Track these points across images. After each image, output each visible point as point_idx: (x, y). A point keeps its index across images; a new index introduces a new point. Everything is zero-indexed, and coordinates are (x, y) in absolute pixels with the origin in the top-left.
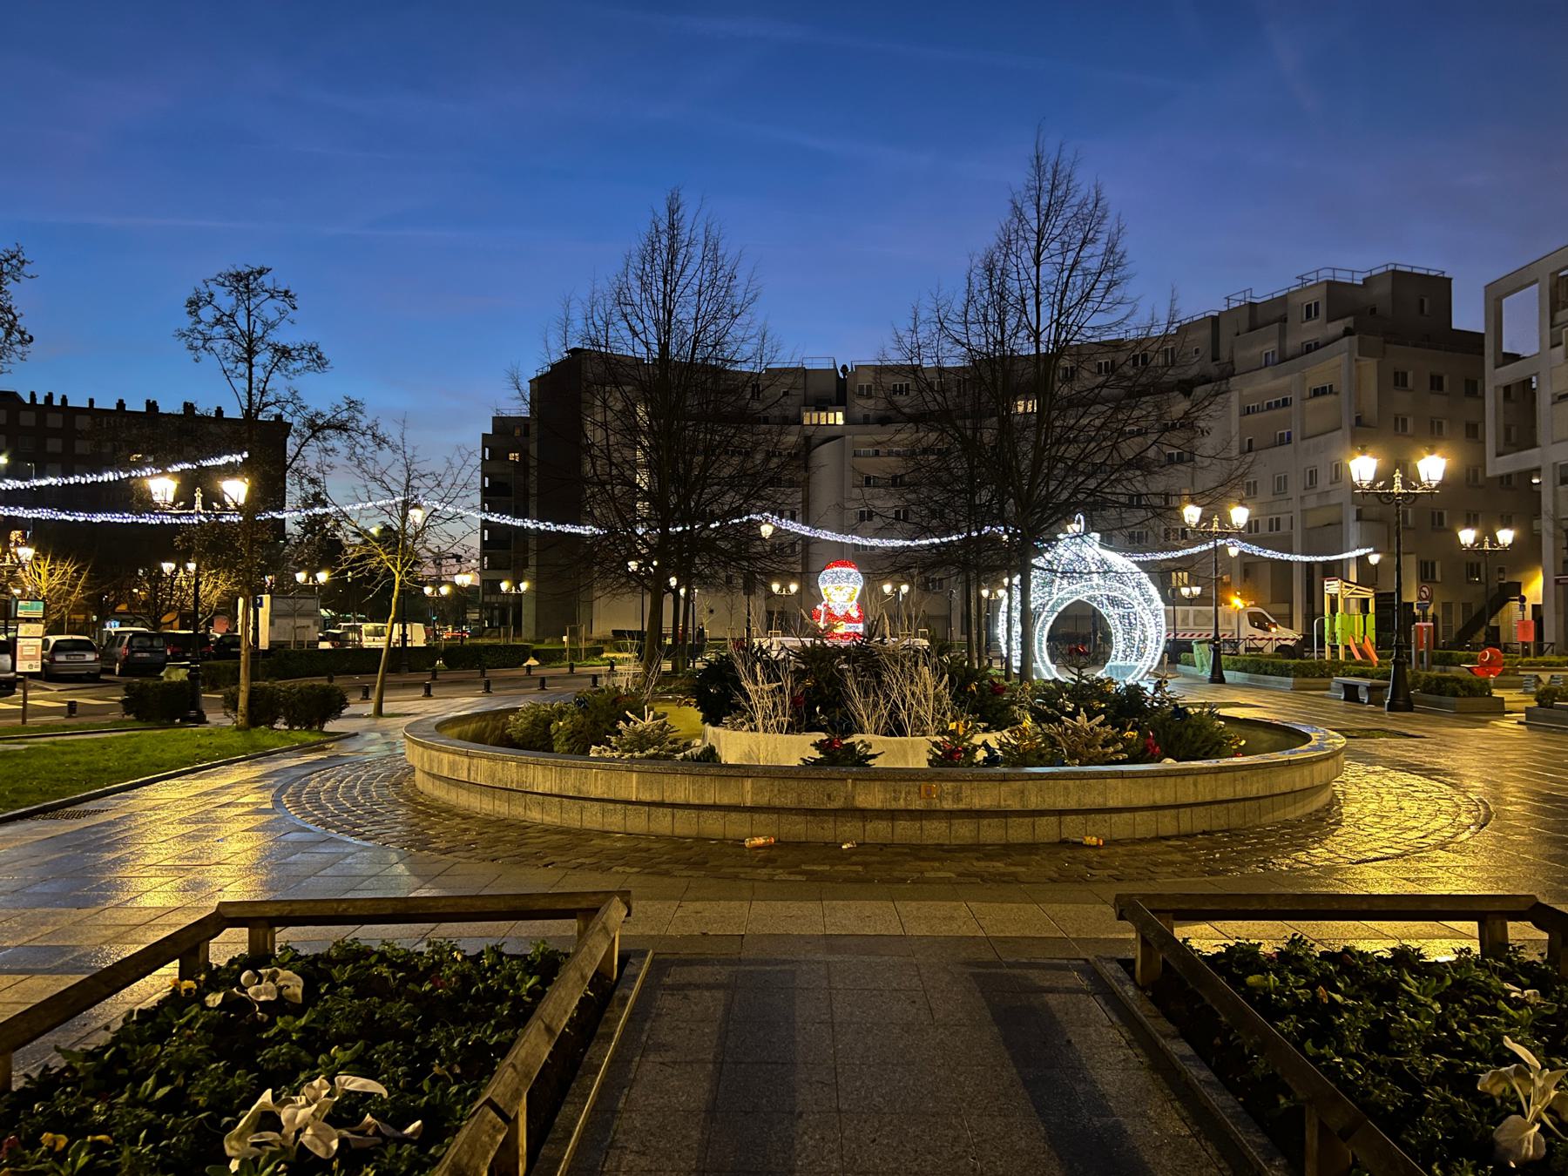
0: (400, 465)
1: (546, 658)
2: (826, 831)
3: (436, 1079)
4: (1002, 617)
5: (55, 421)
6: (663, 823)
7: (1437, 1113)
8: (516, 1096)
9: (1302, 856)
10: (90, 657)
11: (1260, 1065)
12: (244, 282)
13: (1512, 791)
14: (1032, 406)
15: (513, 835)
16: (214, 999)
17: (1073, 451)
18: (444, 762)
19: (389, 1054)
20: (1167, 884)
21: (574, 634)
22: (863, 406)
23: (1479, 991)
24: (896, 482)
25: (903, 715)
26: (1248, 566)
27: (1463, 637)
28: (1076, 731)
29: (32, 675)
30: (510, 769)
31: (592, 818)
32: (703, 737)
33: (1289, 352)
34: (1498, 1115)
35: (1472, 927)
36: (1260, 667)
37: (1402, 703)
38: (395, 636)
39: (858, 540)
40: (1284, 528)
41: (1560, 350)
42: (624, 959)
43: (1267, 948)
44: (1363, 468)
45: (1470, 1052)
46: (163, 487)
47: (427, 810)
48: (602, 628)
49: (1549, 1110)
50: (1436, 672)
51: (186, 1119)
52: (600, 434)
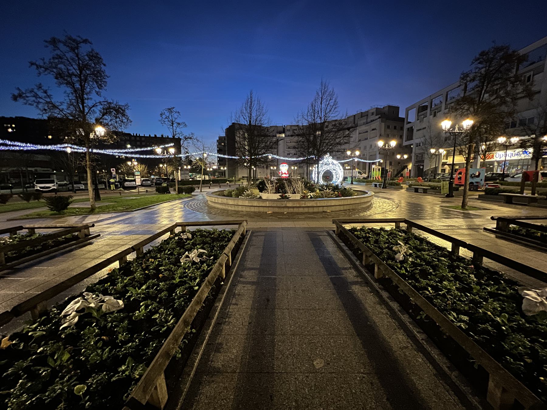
0: (202, 146)
1: (230, 181)
2: (281, 210)
3: (215, 250)
4: (314, 173)
5: (138, 139)
6: (253, 209)
7: (386, 253)
8: (229, 252)
9: (365, 213)
10: (149, 182)
11: (356, 247)
12: (170, 110)
13: (403, 202)
14: (320, 133)
15: (226, 212)
16: (177, 238)
17: (327, 141)
18: (213, 199)
19: (207, 246)
20: (341, 218)
21: (235, 177)
22: (288, 133)
23: (394, 234)
24: (294, 148)
25: (295, 190)
26: (359, 163)
27: (396, 175)
28: (326, 192)
29: (139, 185)
30: (225, 200)
31: (240, 209)
32: (259, 195)
33: (368, 122)
34: (396, 253)
35: (394, 224)
36: (359, 181)
37: (385, 187)
38: (203, 178)
39: (287, 159)
40: (365, 156)
41: (419, 121)
42: (247, 231)
43: (358, 228)
44: (381, 143)
45: (392, 244)
46: (159, 150)
47: (211, 208)
48: (240, 176)
49: (405, 253)
50: (391, 181)
51: (174, 257)
52: (238, 139)
